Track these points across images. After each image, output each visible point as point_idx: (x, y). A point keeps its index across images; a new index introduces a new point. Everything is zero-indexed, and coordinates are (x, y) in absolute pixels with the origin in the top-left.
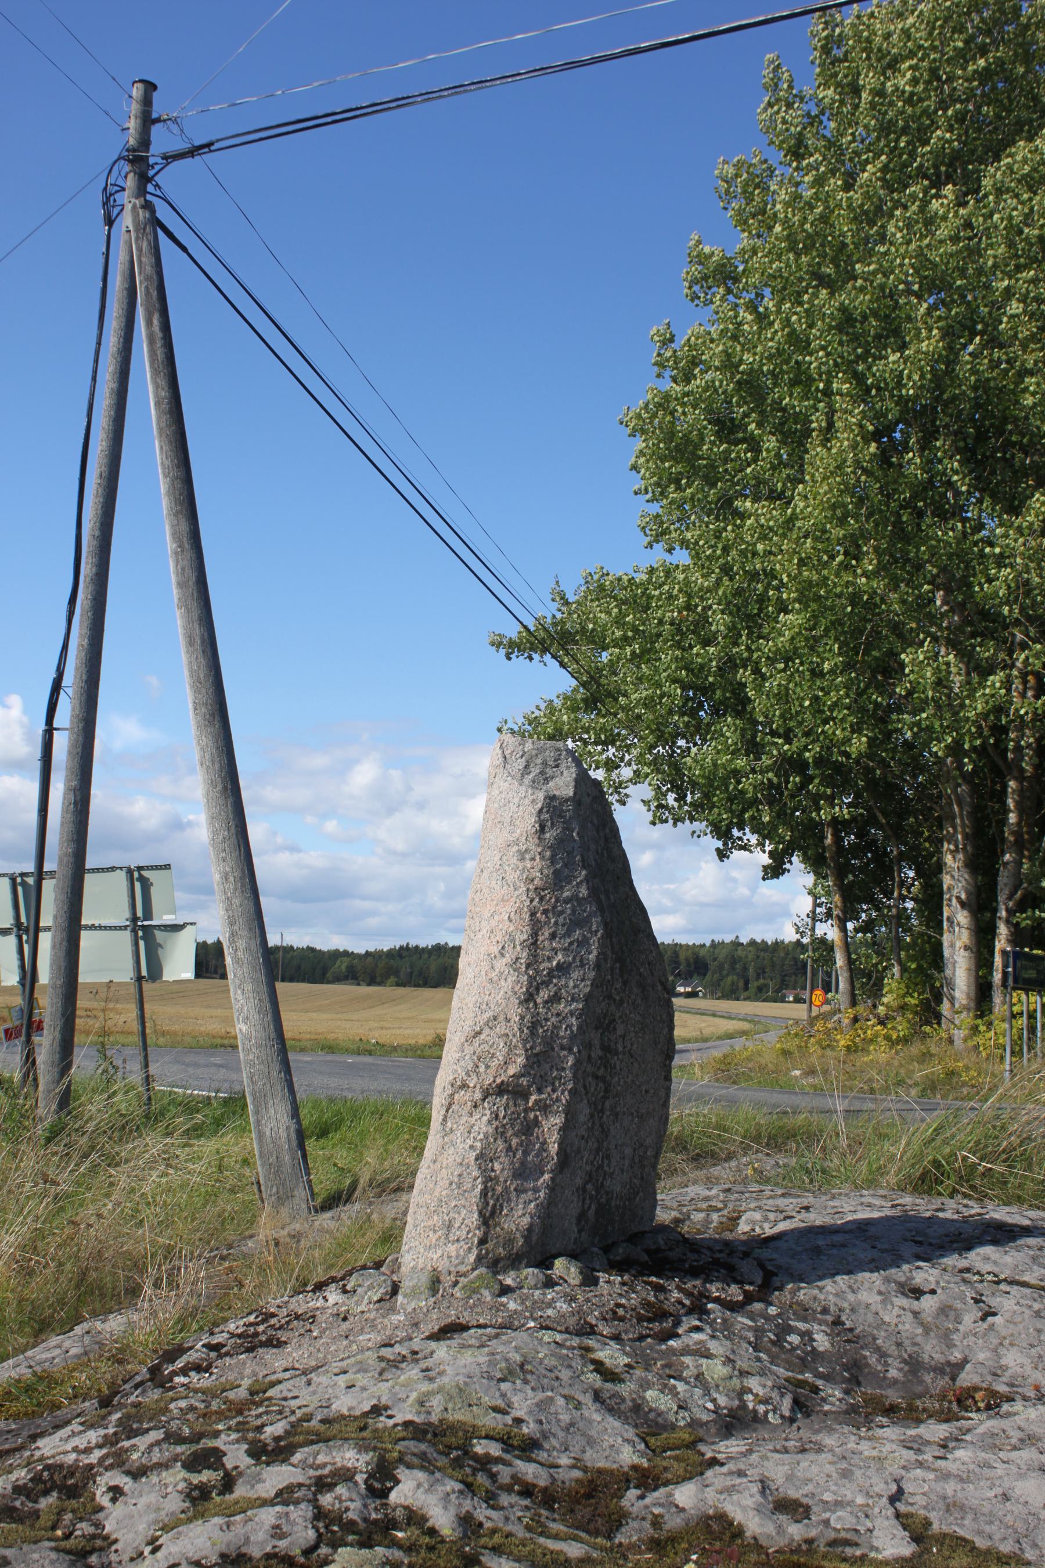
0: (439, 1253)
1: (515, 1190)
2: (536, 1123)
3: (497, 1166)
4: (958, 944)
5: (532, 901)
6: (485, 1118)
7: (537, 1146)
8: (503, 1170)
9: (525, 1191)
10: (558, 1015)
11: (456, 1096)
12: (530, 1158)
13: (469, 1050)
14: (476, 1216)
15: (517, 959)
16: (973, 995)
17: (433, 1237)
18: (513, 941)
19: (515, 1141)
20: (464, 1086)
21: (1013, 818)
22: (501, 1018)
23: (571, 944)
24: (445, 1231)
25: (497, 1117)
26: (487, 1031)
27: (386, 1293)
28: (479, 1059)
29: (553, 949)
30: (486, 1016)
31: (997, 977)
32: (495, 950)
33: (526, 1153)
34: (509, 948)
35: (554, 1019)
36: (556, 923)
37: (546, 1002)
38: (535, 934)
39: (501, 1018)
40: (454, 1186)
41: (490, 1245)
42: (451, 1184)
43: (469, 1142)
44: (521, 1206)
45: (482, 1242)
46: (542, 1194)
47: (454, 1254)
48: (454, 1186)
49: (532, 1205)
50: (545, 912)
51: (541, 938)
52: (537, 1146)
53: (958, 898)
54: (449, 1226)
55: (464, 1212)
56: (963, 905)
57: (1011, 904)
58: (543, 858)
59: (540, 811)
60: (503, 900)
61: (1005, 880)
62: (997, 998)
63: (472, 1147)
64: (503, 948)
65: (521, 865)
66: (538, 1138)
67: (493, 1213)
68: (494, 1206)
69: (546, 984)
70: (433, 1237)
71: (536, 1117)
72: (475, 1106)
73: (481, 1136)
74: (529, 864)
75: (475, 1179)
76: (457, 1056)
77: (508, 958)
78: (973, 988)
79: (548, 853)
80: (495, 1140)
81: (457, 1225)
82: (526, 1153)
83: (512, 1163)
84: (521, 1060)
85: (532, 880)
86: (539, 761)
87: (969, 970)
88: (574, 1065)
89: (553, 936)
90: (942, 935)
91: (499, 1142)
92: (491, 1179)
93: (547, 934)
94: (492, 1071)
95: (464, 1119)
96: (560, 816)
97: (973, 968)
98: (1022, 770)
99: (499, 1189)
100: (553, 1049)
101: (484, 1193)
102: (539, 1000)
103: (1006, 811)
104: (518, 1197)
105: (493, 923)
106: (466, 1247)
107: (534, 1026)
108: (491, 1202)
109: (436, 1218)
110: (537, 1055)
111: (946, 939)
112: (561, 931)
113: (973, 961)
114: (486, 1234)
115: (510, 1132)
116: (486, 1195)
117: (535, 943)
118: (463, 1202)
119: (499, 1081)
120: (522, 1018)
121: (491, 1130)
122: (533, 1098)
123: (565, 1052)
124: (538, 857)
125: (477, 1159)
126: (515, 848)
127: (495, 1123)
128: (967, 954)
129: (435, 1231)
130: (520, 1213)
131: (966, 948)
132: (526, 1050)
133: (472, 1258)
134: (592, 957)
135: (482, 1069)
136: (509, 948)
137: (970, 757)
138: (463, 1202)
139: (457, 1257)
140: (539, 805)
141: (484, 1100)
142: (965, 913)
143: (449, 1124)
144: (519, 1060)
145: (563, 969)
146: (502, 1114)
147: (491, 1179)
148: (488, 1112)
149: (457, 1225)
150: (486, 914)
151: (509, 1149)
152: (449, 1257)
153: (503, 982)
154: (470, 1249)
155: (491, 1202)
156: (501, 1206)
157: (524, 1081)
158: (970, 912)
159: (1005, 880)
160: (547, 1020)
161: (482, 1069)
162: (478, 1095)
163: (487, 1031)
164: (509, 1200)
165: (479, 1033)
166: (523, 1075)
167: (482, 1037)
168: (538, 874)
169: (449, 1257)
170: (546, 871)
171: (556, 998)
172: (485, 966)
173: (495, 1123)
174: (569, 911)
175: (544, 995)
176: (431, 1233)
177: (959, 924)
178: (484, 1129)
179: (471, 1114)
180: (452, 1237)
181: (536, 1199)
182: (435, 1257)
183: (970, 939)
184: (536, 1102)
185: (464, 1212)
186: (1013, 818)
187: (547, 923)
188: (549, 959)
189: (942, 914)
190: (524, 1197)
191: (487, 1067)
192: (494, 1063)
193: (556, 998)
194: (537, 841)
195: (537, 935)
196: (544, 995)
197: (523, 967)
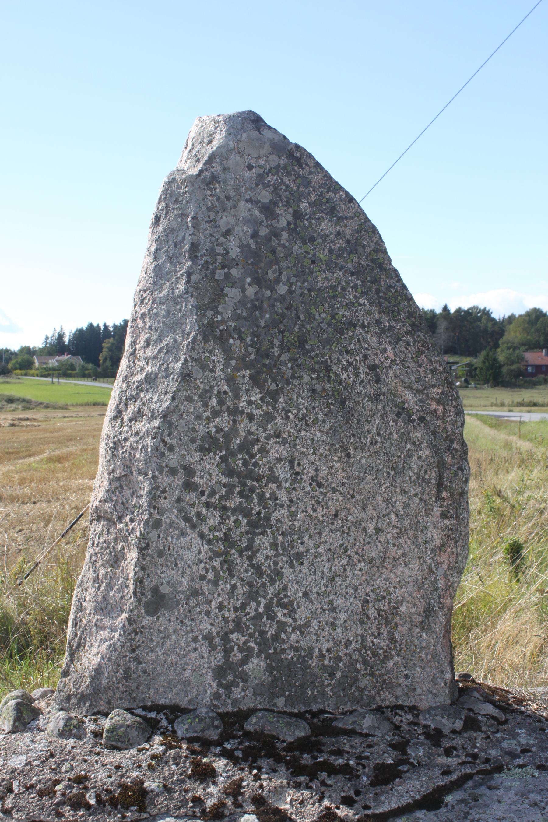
7: (121, 580)
9: (103, 628)
10: (137, 434)
12: (112, 593)
19: (102, 572)
33: (109, 586)
35: (133, 439)
46: (117, 635)
49: (105, 646)
52: (121, 580)
66: (122, 571)
67: (79, 645)
69: (134, 398)
82: (109, 586)
88: (150, 492)
96: (176, 201)
100: (132, 473)
108: (79, 634)
110: (119, 479)
115: (100, 562)
134: (178, 366)
151: (96, 580)
166: (106, 501)
171: (138, 416)
175: (132, 409)
193: (138, 416)
196: (132, 409)
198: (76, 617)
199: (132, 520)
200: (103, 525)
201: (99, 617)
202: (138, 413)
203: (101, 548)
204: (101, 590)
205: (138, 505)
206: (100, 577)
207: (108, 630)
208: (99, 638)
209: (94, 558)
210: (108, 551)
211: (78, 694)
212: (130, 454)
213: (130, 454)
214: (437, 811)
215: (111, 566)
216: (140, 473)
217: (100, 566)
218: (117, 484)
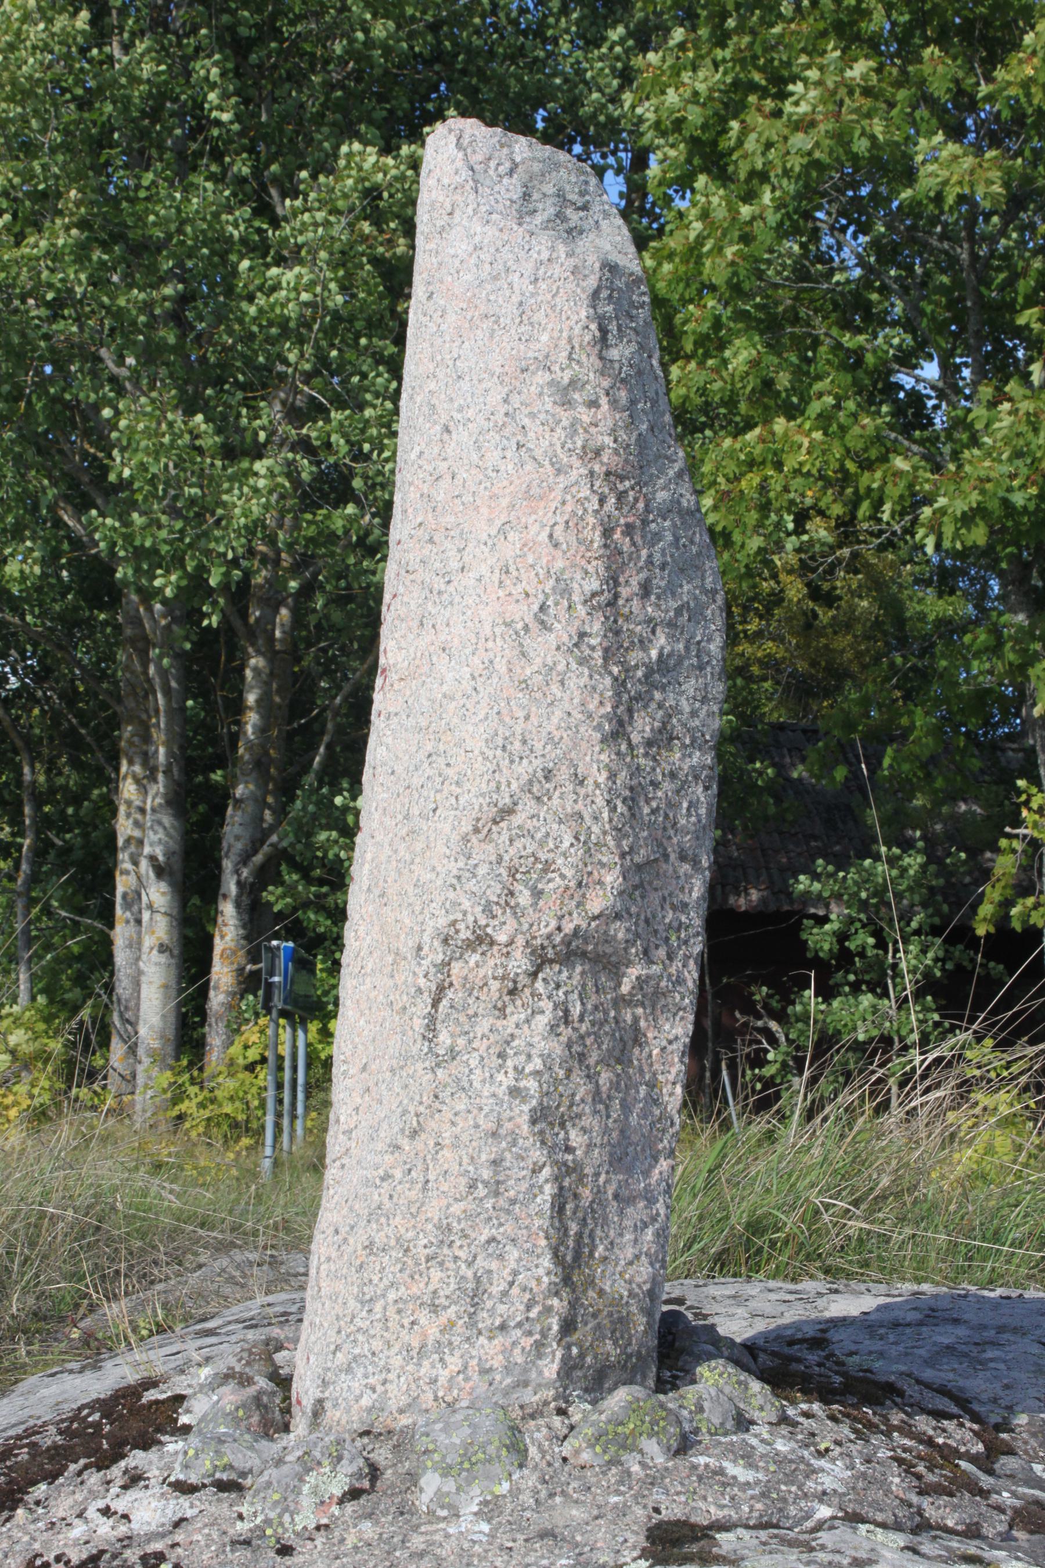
0: (454, 1363)
1: (616, 1196)
2: (637, 1037)
3: (576, 1138)
4: (148, 942)
5: (602, 501)
6: (542, 1022)
8: (590, 1146)
9: (631, 1200)
10: (673, 775)
11: (456, 967)
13: (483, 852)
14: (546, 1262)
15: (582, 635)
16: (171, 1033)
17: (431, 1327)
18: (567, 592)
19: (605, 1077)
20: (481, 940)
21: (252, 720)
22: (563, 774)
23: (679, 611)
24: (464, 1305)
25: (566, 1019)
26: (527, 806)
27: (359, 1475)
28: (513, 873)
29: (649, 620)
30: (524, 769)
31: (217, 1000)
32: (524, 612)
34: (557, 610)
35: (667, 786)
36: (650, 561)
37: (649, 743)
38: (613, 580)
39: (563, 774)
40: (481, 1191)
41: (584, 1332)
42: (472, 1186)
43: (505, 1080)
44: (628, 1237)
45: (568, 1326)
47: (497, 1362)
48: (481, 1191)
50: (629, 530)
51: (624, 592)
52: (643, 1090)
53: (152, 858)
54: (476, 1296)
55: (513, 1254)
56: (160, 871)
57: (245, 873)
58: (614, 403)
59: (595, 295)
60: (528, 495)
61: (237, 830)
62: (215, 1037)
63: (514, 1092)
64: (543, 608)
65: (566, 417)
66: (641, 1071)
68: (579, 1235)
70: (431, 1327)
71: (636, 1020)
72: (512, 992)
73: (537, 1064)
74: (585, 416)
75: (536, 1170)
76: (453, 867)
77: (562, 632)
78: (172, 1019)
79: (623, 395)
80: (569, 1071)
81: (496, 1290)
83: (606, 1131)
84: (612, 878)
85: (598, 453)
86: (549, 189)
87: (166, 987)
89: (646, 589)
90: (111, 926)
91: (578, 1077)
92: (569, 1171)
93: (634, 582)
94: (550, 904)
95: (484, 1025)
97: (173, 983)
98: (271, 639)
99: (586, 1193)
100: (666, 856)
101: (559, 1207)
102: (636, 738)
103: (237, 707)
104: (621, 1213)
105: (509, 550)
106: (528, 1342)
107: (634, 797)
108: (574, 1228)
109: (436, 1274)
110: (639, 868)
111: (121, 934)
112: (659, 582)
113: (173, 972)
114: (573, 1305)
116: (561, 1210)
117: (612, 603)
118: (509, 1228)
119: (568, 927)
120: (612, 776)
121: (557, 1048)
122: (634, 972)
123: (686, 867)
124: (604, 401)
125: (534, 1122)
126: (542, 378)
127: (566, 1032)
128: (163, 959)
129: (435, 1309)
130: (630, 1252)
131: (162, 948)
132: (623, 856)
133: (550, 1368)
135: (524, 898)
136: (557, 610)
137: (215, 603)
138: (509, 1228)
139: (508, 1369)
140: (592, 282)
141: (534, 975)
142: (163, 886)
143: (444, 1038)
144: (609, 879)
145: (665, 665)
146: (576, 1010)
147: (569, 1171)
148: (547, 1005)
149: (496, 1290)
150: (483, 530)
152: (485, 1371)
153: (555, 689)
154: (539, 1345)
155: (574, 1228)
156: (591, 1236)
157: (620, 931)
158: (171, 884)
159: (237, 830)
160: (655, 785)
161: (524, 898)
162: (520, 963)
163: (527, 806)
164: (605, 1222)
165: (508, 812)
166: (618, 916)
167: (517, 819)
168: (608, 440)
169: (485, 1371)
170: (623, 436)
172: (502, 652)
173: (566, 1032)
174: (669, 537)
175: (642, 727)
176: (423, 1317)
177: (150, 907)
178: (542, 1046)
179: (502, 1012)
180: (485, 1320)
181: (654, 1219)
182: (444, 1375)
183: (169, 932)
184: (641, 982)
185: (513, 1254)
186: (252, 720)
187: (634, 557)
188: (644, 644)
189: (113, 892)
190: (637, 1212)
191: (537, 894)
192: (553, 885)
194: (598, 364)
195: (617, 584)
197: (598, 654)
198: (561, 1188)
199: (670, 957)
200: (583, 973)
201: (621, 1177)
202: (660, 731)
203: (593, 1023)
204: (615, 1115)
205: (675, 924)
206: (604, 1089)
207: (641, 1204)
208: (628, 1223)
209: (577, 1048)
210: (607, 1029)
211: (629, 1356)
212: (666, 816)
213: (666, 816)
214: (656, 1518)
215: (619, 1061)
216: (683, 858)
217: (597, 1063)
218: (637, 880)
